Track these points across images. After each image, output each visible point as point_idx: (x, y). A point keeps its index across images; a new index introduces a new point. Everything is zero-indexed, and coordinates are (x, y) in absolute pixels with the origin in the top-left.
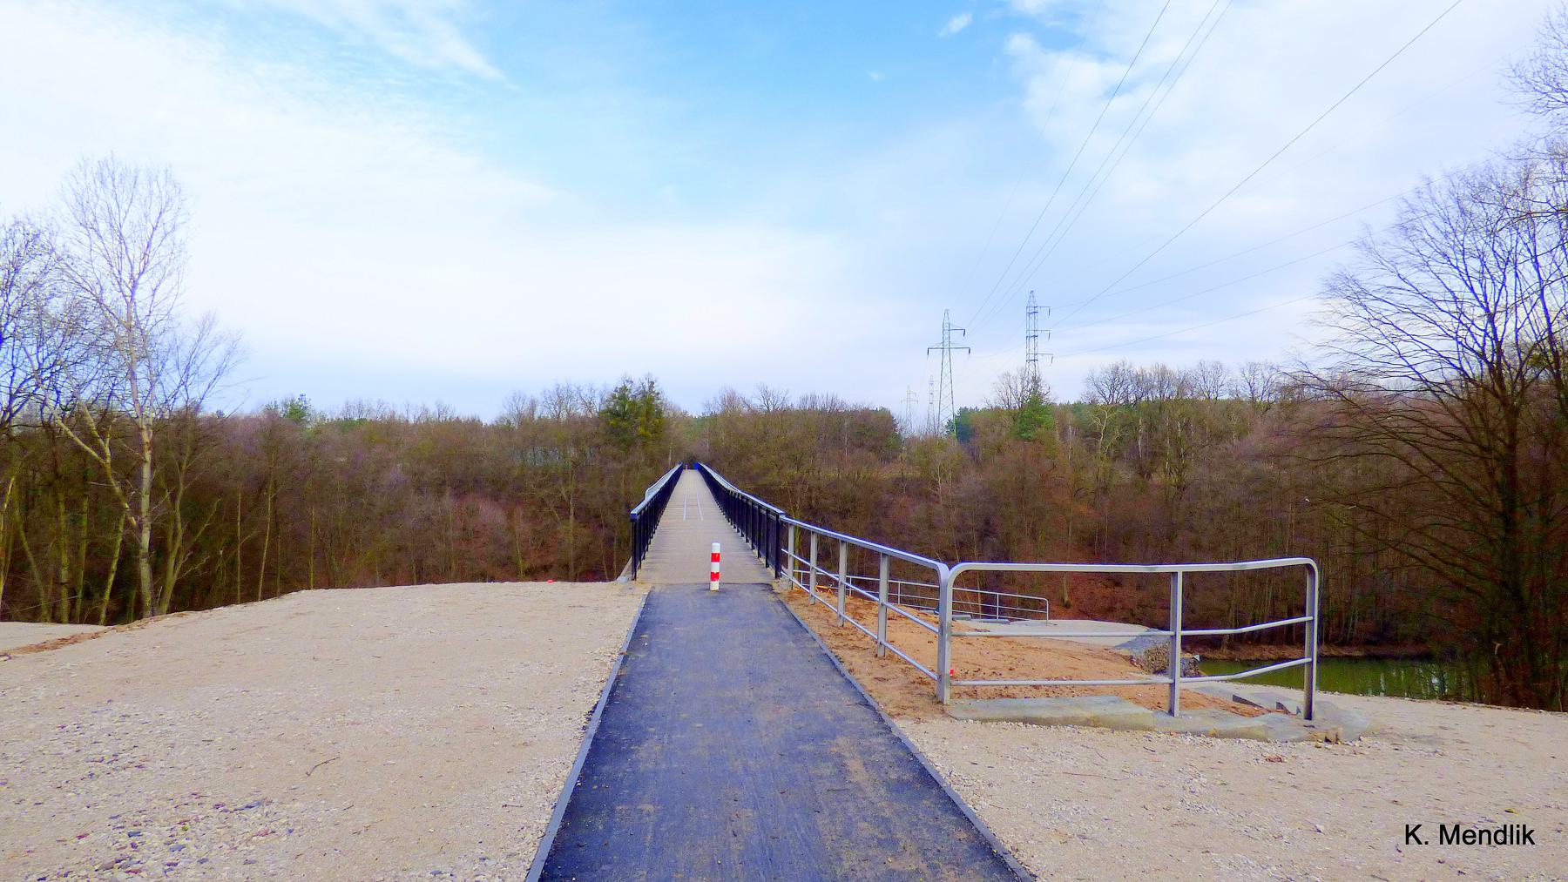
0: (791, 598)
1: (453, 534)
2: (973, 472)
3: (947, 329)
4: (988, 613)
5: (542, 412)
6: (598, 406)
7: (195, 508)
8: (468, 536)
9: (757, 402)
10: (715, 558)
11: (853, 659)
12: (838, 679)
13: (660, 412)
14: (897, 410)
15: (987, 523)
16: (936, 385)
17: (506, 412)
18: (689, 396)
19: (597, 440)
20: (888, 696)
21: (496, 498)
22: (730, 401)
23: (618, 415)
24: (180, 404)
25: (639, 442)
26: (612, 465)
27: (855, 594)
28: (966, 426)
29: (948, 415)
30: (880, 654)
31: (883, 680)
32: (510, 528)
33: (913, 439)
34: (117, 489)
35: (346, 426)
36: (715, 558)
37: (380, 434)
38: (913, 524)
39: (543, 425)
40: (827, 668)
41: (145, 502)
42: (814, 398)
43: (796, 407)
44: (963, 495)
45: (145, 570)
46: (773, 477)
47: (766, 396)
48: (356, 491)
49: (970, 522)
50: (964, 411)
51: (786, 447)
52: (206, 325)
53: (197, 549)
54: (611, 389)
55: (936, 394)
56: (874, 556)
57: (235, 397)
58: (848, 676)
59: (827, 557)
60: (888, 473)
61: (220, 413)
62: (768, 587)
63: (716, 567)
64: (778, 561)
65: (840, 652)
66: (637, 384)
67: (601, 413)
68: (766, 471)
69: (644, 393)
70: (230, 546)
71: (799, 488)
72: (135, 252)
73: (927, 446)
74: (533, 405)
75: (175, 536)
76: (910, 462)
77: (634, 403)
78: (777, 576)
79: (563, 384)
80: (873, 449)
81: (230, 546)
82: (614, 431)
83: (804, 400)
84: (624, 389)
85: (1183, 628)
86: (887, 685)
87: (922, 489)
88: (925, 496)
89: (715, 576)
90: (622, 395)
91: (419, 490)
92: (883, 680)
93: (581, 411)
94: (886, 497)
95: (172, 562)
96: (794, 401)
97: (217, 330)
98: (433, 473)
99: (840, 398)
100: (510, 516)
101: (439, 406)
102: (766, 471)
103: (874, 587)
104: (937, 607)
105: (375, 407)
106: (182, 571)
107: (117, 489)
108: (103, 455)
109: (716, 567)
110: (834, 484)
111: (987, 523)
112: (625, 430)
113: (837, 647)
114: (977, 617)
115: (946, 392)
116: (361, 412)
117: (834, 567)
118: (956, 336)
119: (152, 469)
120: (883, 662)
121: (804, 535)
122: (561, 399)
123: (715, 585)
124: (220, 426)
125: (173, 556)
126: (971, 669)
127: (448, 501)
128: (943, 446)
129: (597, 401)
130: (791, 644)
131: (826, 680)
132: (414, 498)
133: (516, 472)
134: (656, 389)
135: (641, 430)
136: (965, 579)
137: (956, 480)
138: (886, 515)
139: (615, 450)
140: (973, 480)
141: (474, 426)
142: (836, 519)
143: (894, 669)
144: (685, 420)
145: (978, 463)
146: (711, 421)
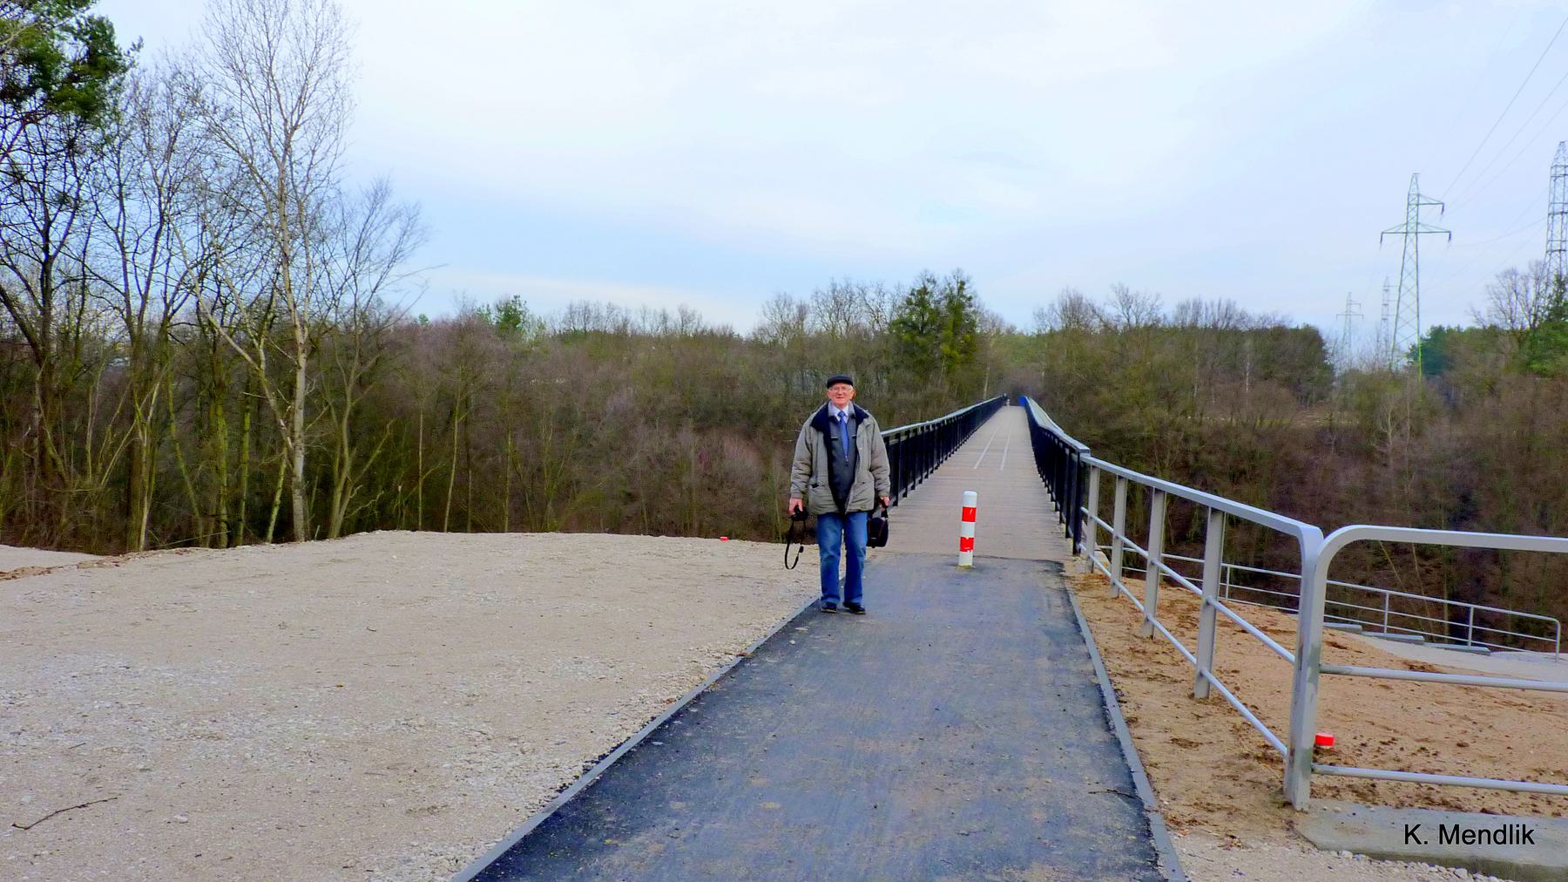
0: (1086, 587)
1: (691, 479)
2: (1445, 421)
3: (1415, 202)
4: (1457, 635)
5: (815, 324)
6: (888, 314)
7: (363, 428)
8: (715, 483)
9: (1112, 311)
10: (969, 515)
11: (1149, 699)
12: (1097, 735)
13: (973, 324)
14: (1328, 325)
15: (1465, 499)
16: (1394, 291)
17: (767, 321)
18: (1015, 304)
19: (883, 361)
20: (1180, 780)
21: (749, 436)
22: (1074, 310)
23: (914, 326)
24: (347, 300)
25: (943, 365)
26: (904, 396)
27: (1170, 582)
28: (1439, 351)
29: (1410, 336)
30: (1200, 694)
31: (1188, 744)
32: (765, 477)
33: (1353, 373)
34: (272, 402)
35: (569, 338)
36: (969, 515)
37: (600, 345)
38: (1343, 496)
39: (818, 342)
40: (1087, 710)
41: (299, 418)
42: (1197, 306)
43: (1171, 318)
44: (1426, 455)
45: (299, 503)
46: (1132, 419)
47: (1126, 301)
48: (565, 421)
49: (1437, 497)
50: (1438, 332)
51: (1150, 376)
52: (378, 196)
53: (370, 484)
54: (906, 291)
55: (1393, 305)
56: (1148, 491)
57: (428, 290)
58: (1121, 731)
59: (1186, 530)
60: (1309, 420)
61: (423, 318)
62: (1058, 568)
63: (969, 530)
64: (1074, 522)
65: (1126, 685)
66: (941, 284)
67: (893, 324)
68: (1121, 410)
69: (951, 298)
70: (412, 478)
71: (1170, 435)
72: (289, 101)
73: (1372, 386)
74: (802, 312)
75: (341, 465)
76: (1344, 407)
77: (937, 312)
78: (1076, 552)
79: (841, 284)
80: (1287, 382)
81: (412, 478)
82: (909, 350)
83: (1183, 308)
84: (924, 291)
85: (1391, 597)
86: (1191, 755)
87: (1362, 447)
88: (1368, 455)
89: (966, 544)
90: (920, 298)
91: (650, 421)
92: (1188, 744)
93: (865, 321)
94: (1303, 455)
95: (338, 496)
96: (1168, 312)
97: (391, 203)
98: (671, 399)
99: (1239, 308)
100: (765, 460)
101: (683, 313)
102: (1121, 410)
103: (1195, 573)
104: (1291, 604)
105: (604, 313)
106: (352, 505)
107: (272, 402)
108: (257, 360)
109: (969, 530)
110: (1220, 433)
111: (1465, 499)
112: (923, 349)
113: (1126, 675)
114: (1440, 640)
115: (1409, 299)
116: (587, 320)
117: (1143, 540)
118: (1428, 215)
119: (307, 379)
120: (1201, 710)
121: (1108, 480)
122: (839, 302)
123: (967, 558)
124: (415, 333)
125: (339, 489)
126: (1375, 737)
127: (688, 438)
128: (1396, 379)
129: (888, 308)
130: (1044, 663)
131: (1072, 736)
132: (642, 431)
133: (776, 402)
134: (967, 292)
135: (945, 348)
136: (1346, 562)
137: (1417, 433)
138: (1302, 482)
139: (909, 376)
140: (1445, 435)
141: (724, 341)
142: (1225, 483)
143: (1219, 723)
144: (1012, 340)
145: (1457, 414)
146: (1045, 342)
